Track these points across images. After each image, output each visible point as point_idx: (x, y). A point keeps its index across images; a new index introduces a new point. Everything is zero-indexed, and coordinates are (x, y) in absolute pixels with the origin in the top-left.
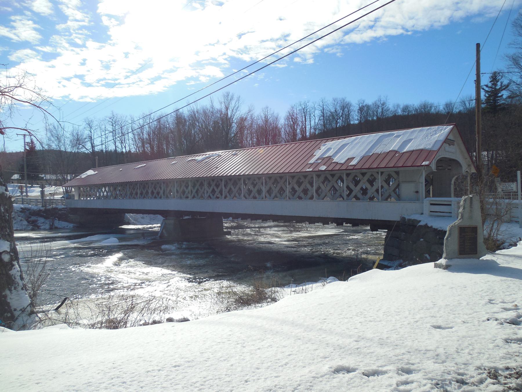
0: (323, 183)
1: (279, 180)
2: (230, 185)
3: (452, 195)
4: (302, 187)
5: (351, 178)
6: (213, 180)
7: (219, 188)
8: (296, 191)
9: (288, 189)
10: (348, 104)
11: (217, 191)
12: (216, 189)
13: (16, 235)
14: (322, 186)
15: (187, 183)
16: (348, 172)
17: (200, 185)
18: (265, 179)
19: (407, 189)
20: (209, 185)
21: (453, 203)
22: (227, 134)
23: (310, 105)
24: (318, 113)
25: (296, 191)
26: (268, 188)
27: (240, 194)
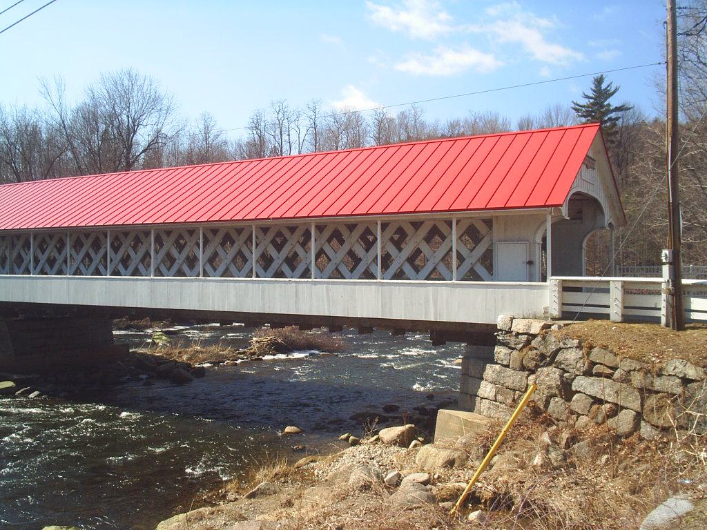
0: (428, 239)
1: (234, 235)
2: (169, 245)
3: (313, 276)
4: (285, 251)
5: (357, 233)
6: (51, 237)
7: (102, 252)
8: (360, 260)
9: (254, 256)
10: (557, 106)
11: (97, 258)
12: (93, 254)
13: (460, 368)
14: (425, 248)
15: (368, 232)
16: (385, 218)
17: (23, 247)
18: (205, 236)
19: (508, 255)
20: (78, 245)
21: (612, 286)
22: (129, 146)
23: (291, 108)
24: (305, 123)
25: (360, 260)
26: (209, 252)
27: (148, 267)
